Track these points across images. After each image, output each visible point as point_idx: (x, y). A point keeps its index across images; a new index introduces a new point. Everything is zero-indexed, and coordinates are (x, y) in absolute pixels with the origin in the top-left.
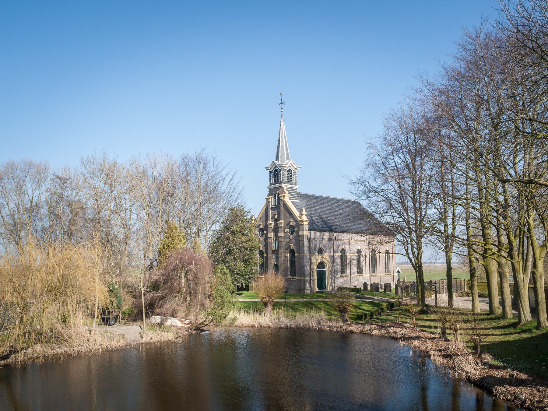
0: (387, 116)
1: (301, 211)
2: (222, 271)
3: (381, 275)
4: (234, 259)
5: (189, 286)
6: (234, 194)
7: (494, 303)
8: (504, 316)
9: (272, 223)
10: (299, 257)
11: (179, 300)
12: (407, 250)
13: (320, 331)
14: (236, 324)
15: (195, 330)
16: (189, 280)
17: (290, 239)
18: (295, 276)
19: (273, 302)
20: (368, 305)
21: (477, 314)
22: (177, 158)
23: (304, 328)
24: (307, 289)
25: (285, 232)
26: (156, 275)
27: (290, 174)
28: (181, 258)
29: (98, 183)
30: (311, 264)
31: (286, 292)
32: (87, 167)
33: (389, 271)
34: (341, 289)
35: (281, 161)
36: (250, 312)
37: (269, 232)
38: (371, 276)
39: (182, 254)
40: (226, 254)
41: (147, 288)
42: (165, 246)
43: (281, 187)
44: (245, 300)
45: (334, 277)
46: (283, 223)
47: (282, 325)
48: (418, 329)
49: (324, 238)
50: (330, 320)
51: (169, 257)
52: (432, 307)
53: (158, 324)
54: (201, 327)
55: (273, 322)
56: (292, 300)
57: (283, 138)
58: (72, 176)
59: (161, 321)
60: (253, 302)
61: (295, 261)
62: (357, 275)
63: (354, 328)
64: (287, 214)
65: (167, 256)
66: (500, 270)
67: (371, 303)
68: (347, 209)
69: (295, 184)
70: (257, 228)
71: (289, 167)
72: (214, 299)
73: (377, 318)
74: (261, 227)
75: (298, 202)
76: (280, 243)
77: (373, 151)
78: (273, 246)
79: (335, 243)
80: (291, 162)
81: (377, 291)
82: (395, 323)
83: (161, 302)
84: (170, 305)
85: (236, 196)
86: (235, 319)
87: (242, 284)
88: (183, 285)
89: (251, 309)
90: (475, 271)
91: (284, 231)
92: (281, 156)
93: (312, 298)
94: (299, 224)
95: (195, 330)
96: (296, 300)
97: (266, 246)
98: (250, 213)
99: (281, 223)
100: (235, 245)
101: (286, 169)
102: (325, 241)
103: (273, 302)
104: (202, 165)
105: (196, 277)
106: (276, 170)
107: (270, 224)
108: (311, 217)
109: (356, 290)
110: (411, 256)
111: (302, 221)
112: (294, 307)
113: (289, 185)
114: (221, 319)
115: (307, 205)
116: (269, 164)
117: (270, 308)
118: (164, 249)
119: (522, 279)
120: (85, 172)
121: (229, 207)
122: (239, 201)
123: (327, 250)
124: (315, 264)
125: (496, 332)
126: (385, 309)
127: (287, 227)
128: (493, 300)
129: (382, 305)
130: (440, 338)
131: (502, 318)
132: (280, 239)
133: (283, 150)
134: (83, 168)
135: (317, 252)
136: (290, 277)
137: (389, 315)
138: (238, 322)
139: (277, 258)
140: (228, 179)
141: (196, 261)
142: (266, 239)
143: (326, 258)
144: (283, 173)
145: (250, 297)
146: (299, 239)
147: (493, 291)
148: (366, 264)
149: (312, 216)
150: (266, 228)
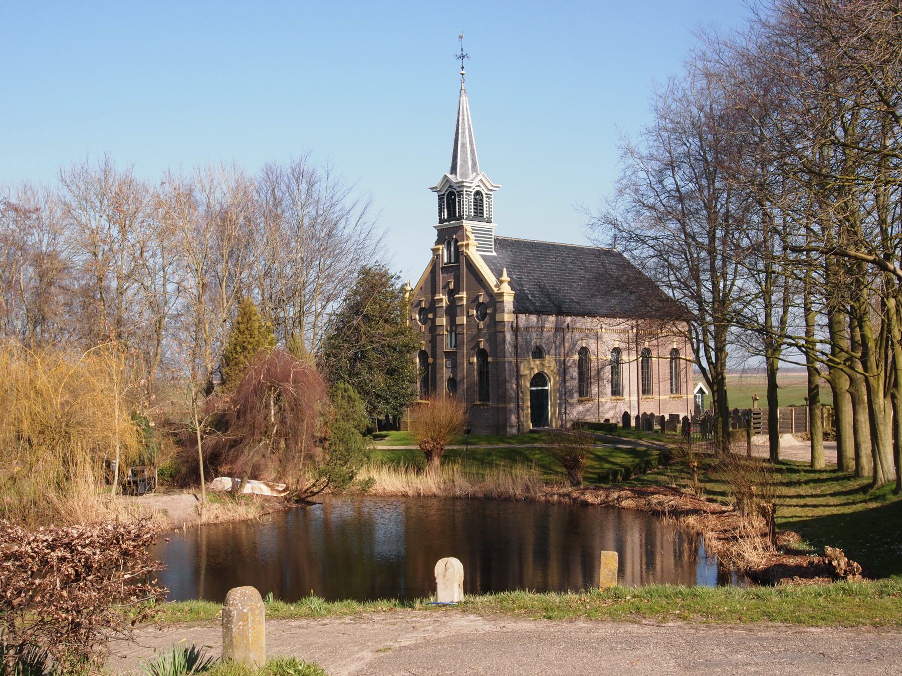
0: (662, 91)
1: (498, 275)
2: (346, 394)
3: (661, 397)
4: (370, 368)
5: (283, 422)
6: (367, 243)
7: (846, 451)
8: (857, 474)
9: (444, 297)
10: (496, 363)
11: (267, 445)
12: (696, 352)
13: (530, 501)
14: (374, 492)
15: (297, 502)
16: (284, 411)
17: (478, 328)
18: (489, 401)
19: (442, 449)
20: (626, 456)
21: (820, 471)
22: (254, 171)
23: (499, 497)
24: (512, 426)
25: (468, 316)
26: (223, 401)
27: (479, 202)
28: (268, 370)
29: (97, 220)
30: (519, 376)
31: (468, 432)
32: (74, 188)
33: (678, 390)
34: (579, 425)
35: (461, 175)
36: (399, 468)
37: (438, 316)
38: (640, 401)
39: (271, 363)
40: (354, 360)
41: (207, 427)
42: (238, 349)
43: (461, 227)
44: (390, 448)
45: (564, 403)
46: (465, 299)
47: (458, 493)
48: (704, 497)
49: (546, 326)
50: (547, 483)
51: (245, 368)
52: (740, 458)
53: (229, 492)
54: (307, 497)
55: (442, 487)
56: (483, 446)
57: (464, 129)
58: (41, 205)
59: (233, 487)
60: (406, 450)
61: (487, 372)
62: (613, 398)
63: (589, 498)
64: (473, 280)
65: (242, 366)
66: (852, 390)
67: (632, 452)
68: (594, 267)
69: (489, 221)
70: (416, 306)
71: (477, 186)
72: (330, 445)
73: (637, 480)
74: (423, 305)
75: (494, 257)
76: (459, 337)
77: (631, 161)
78: (446, 344)
79: (568, 336)
80: (480, 177)
81: (649, 430)
82: (666, 487)
83: (231, 453)
84: (249, 456)
85: (372, 247)
86: (370, 482)
87: (387, 416)
88: (273, 419)
89: (402, 463)
90: (818, 391)
91: (468, 313)
92: (461, 164)
93: (522, 442)
94: (495, 300)
95: (297, 502)
96: (490, 447)
97: (433, 342)
98: (400, 280)
99: (461, 298)
100: (372, 342)
101: (471, 192)
102: (548, 334)
103: (442, 449)
104: (304, 186)
105: (296, 405)
106: (451, 194)
107: (441, 300)
108: (522, 285)
109: (607, 426)
110: (705, 364)
111: (501, 294)
112: (484, 460)
113: (476, 224)
114: (343, 481)
115: (513, 261)
116: (437, 182)
117: (436, 461)
118: (236, 353)
119: (882, 407)
120: (69, 198)
121: (358, 268)
122: (377, 257)
123: (553, 351)
124: (529, 378)
125: (833, 501)
126: (653, 462)
127: (472, 305)
128: (843, 445)
129: (650, 455)
130: (734, 510)
131: (853, 477)
132: (459, 330)
133: (464, 152)
134: (65, 191)
135: (530, 354)
136: (478, 403)
137: (658, 474)
138: (377, 488)
139: (454, 367)
140: (357, 212)
141: (296, 373)
142: (433, 328)
143: (550, 365)
144: (465, 200)
145: (403, 442)
146: (496, 327)
147: (844, 429)
148: (630, 375)
149: (522, 285)
150: (433, 306)
